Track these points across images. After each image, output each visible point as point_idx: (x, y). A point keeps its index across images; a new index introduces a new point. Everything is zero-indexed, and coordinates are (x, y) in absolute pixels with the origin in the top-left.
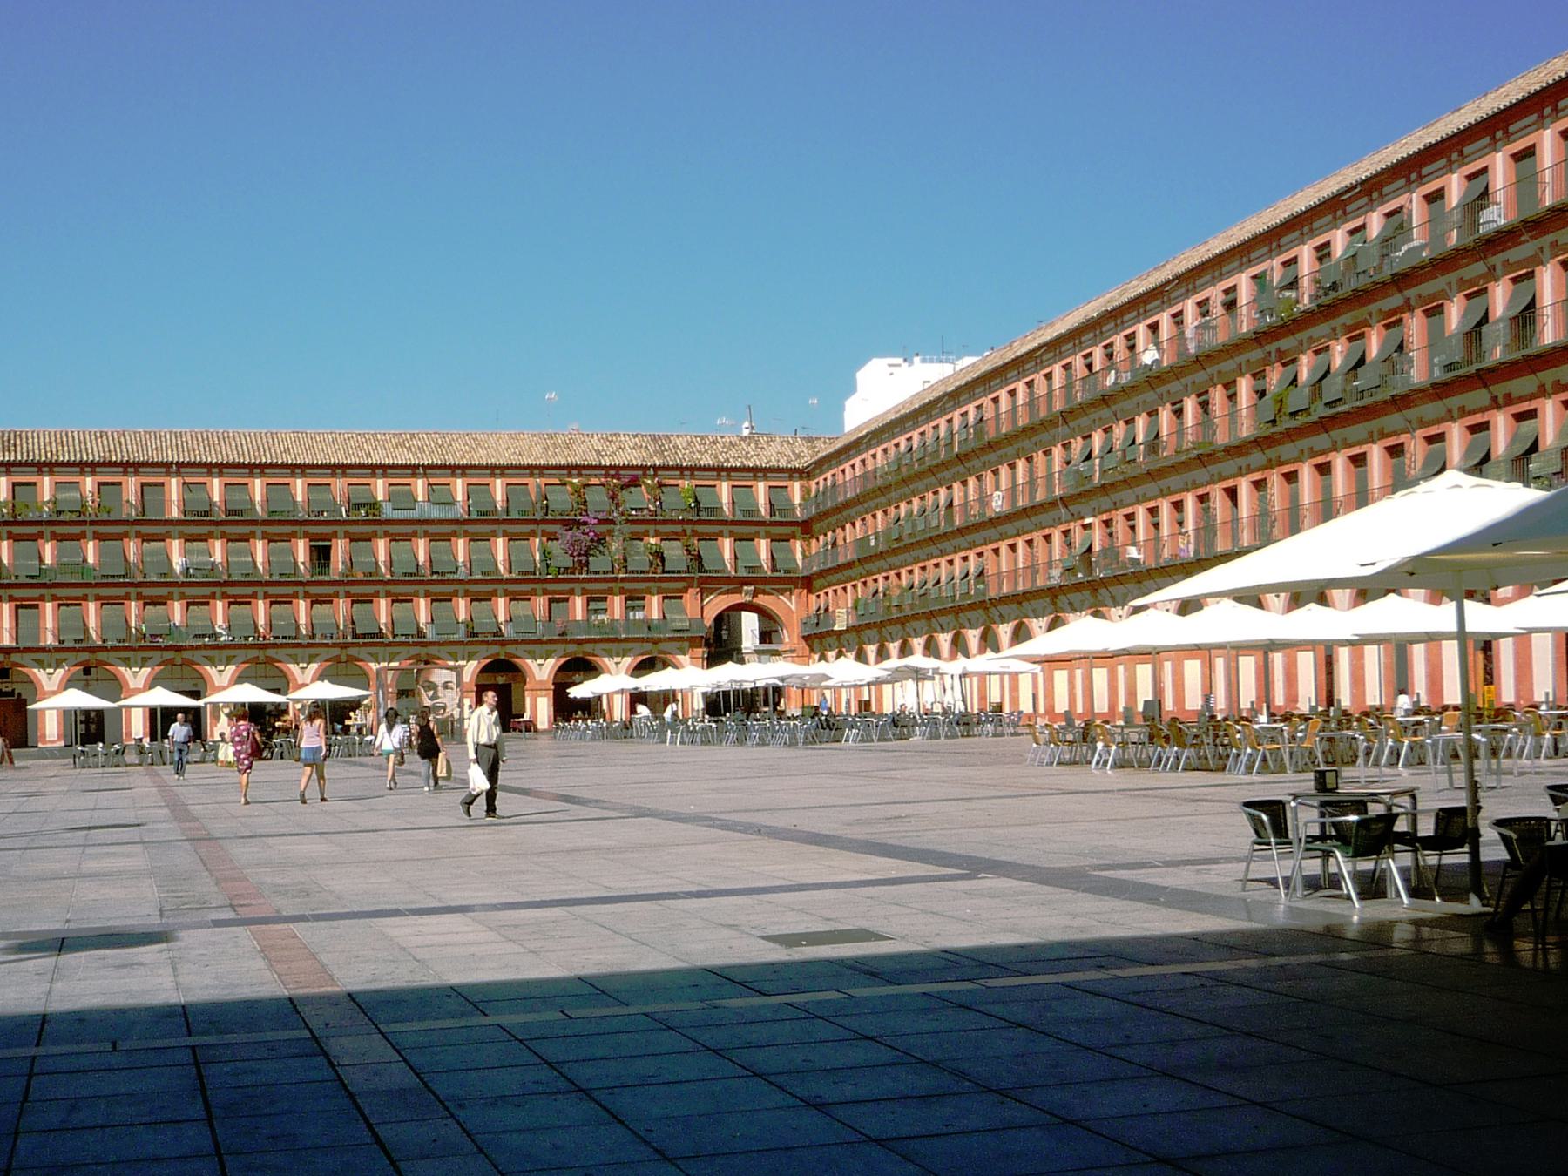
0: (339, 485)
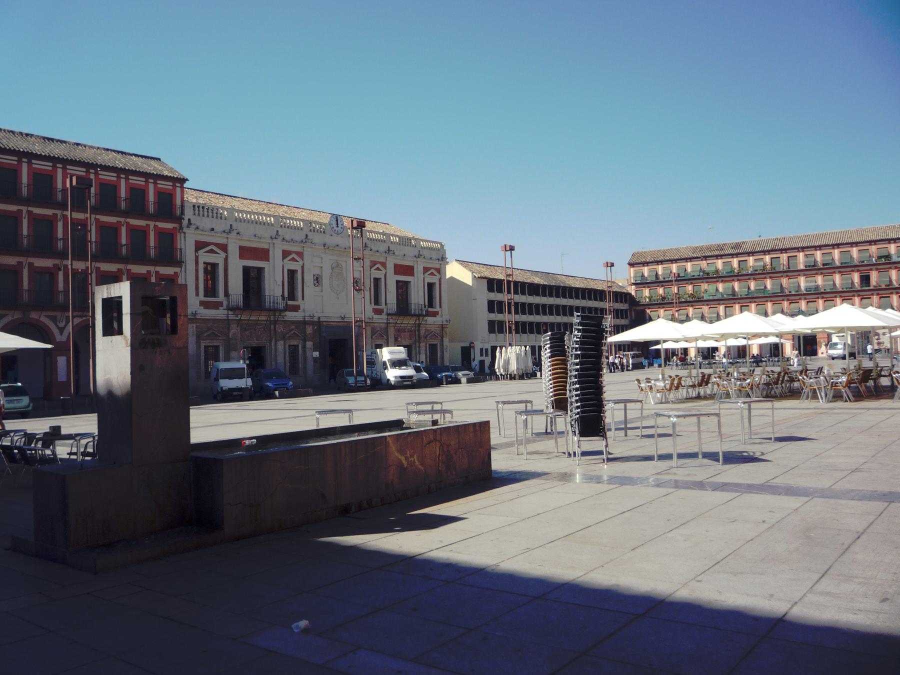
0: (873, 249)
